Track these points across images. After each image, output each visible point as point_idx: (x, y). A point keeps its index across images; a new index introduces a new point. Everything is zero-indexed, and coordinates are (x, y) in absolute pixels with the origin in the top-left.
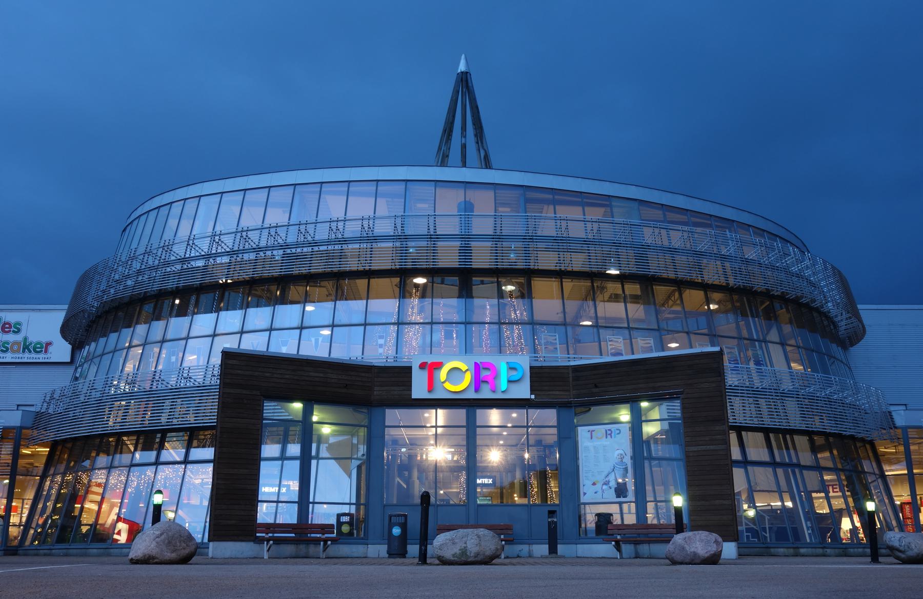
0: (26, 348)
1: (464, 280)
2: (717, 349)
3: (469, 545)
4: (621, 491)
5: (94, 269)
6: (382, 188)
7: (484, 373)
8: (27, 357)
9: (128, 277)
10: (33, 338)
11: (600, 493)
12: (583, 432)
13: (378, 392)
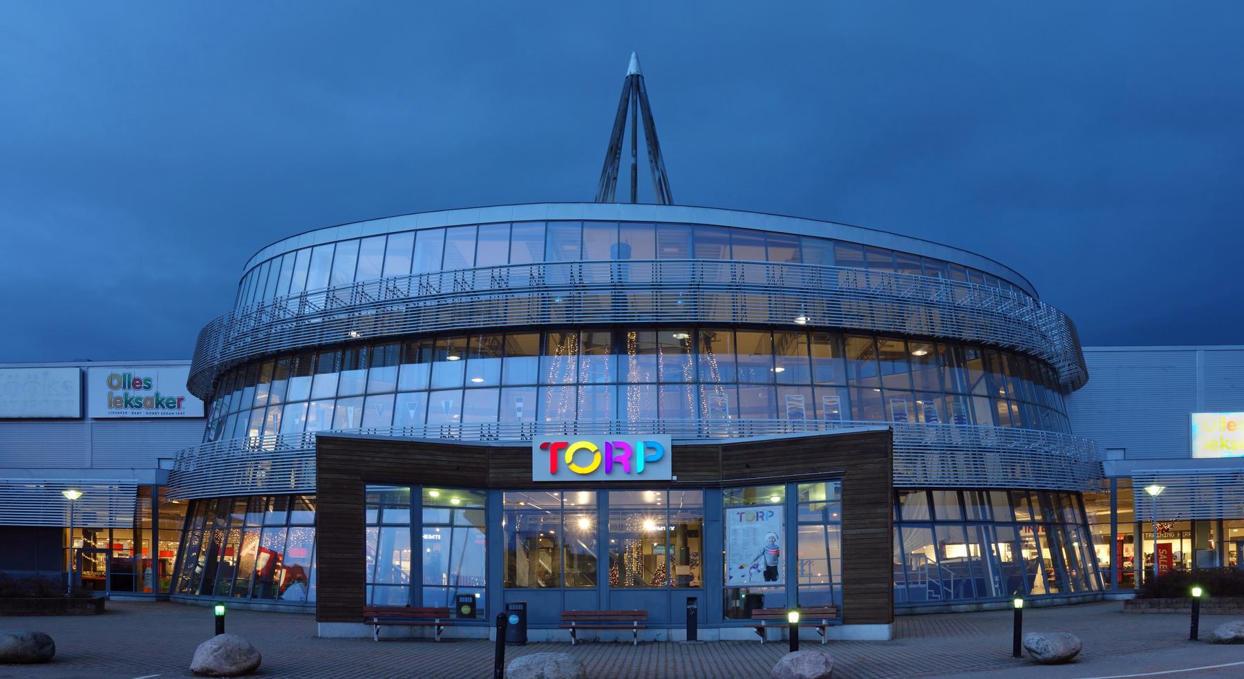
0: (159, 403)
1: (619, 336)
2: (886, 428)
3: (546, 671)
4: (771, 573)
5: (211, 325)
6: (517, 229)
7: (617, 454)
8: (161, 412)
9: (245, 335)
10: (165, 394)
11: (747, 576)
12: (731, 515)
13: (493, 475)
